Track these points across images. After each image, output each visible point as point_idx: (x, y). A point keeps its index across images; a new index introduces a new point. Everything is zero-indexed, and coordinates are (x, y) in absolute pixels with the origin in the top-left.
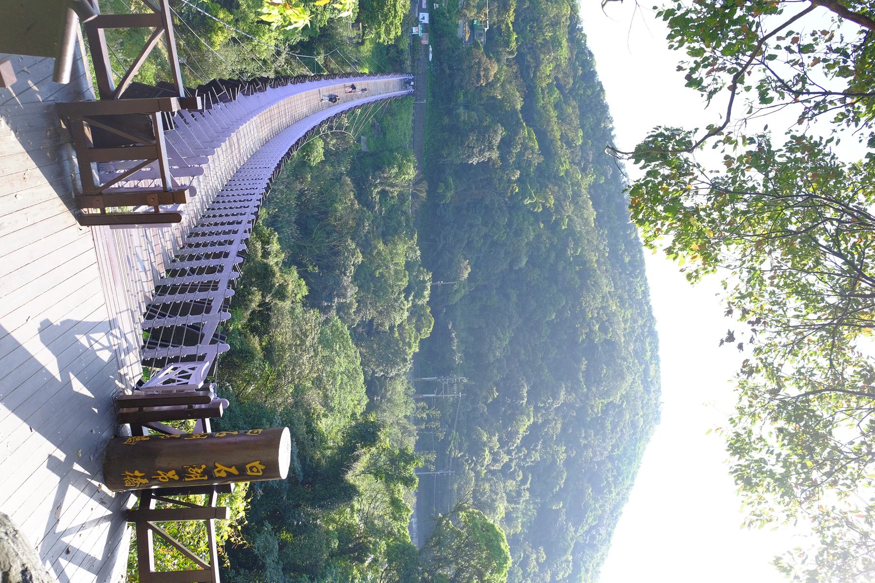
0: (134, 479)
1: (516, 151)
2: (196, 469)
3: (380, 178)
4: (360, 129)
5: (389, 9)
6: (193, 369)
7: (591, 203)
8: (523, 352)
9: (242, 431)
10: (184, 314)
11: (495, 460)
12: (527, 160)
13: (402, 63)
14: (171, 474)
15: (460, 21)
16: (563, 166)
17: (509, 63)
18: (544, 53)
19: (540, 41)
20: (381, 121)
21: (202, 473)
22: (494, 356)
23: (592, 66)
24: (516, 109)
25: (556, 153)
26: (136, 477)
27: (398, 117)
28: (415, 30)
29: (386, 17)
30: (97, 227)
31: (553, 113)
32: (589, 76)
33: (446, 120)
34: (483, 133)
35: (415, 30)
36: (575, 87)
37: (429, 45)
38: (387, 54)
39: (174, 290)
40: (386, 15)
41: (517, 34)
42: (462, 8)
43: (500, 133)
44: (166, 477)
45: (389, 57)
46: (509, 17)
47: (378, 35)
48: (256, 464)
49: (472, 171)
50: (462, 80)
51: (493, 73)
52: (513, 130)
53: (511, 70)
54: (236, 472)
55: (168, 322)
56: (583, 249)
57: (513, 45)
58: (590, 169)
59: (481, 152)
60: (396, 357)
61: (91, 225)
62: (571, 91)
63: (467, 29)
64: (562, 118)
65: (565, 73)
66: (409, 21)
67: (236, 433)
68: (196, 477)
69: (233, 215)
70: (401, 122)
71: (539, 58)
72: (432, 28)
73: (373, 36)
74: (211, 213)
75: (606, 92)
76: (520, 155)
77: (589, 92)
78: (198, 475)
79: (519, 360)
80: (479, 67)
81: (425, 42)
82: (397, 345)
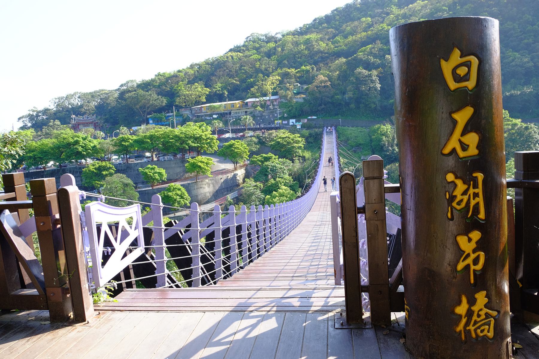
0: (475, 318)
1: (372, 59)
2: (458, 192)
3: (388, 147)
4: (356, 159)
5: (285, 141)
7: (411, 5)
8: (526, 41)
12: (379, 51)
13: (317, 134)
15: (294, 100)
16: (385, 28)
17: (319, 69)
18: (313, 49)
19: (306, 52)
20: (352, 147)
22: (528, 62)
23: (322, 18)
24: (346, 62)
25: (376, 34)
26: (470, 313)
27: (350, 136)
29: (289, 143)
31: (350, 38)
32: (328, 19)
33: (353, 106)
34: (360, 81)
36: (334, 27)
37: (307, 119)
38: (312, 143)
40: (288, 143)
41: (302, 66)
42: (287, 100)
43: (361, 71)
44: (473, 256)
45: (314, 142)
46: (292, 72)
47: (300, 148)
48: (447, 67)
49: (385, 87)
50: (328, 97)
51: (323, 78)
52: (359, 63)
53: (322, 68)
56: (443, 5)
57: (308, 68)
58: (387, 10)
59: (373, 81)
60: (524, 135)
62: (336, 29)
63: (299, 96)
64: (353, 32)
65: (326, 35)
66: (293, 130)
68: (476, 195)
70: (353, 134)
71: (316, 51)
72: (298, 117)
73: (300, 151)
75: (338, 7)
76: (375, 56)
77: (338, 17)
78: (471, 191)
79: (533, 43)
80: (320, 86)
81: (306, 121)
82: (513, 134)
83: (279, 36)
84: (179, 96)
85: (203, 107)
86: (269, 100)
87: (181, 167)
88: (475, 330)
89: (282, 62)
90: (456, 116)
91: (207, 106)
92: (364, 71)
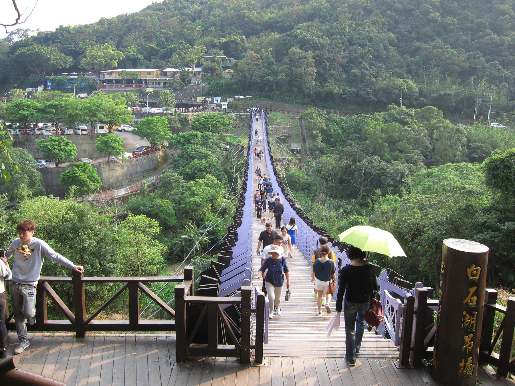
14: (467, 339)
26: (465, 366)
28: (224, 107)
35: (224, 107)
48: (469, 270)
54: (475, 288)
68: (473, 320)
84: (85, 57)
85: (114, 72)
86: (192, 72)
87: (90, 143)
88: (466, 373)
89: (208, 29)
90: (470, 289)
91: (118, 72)
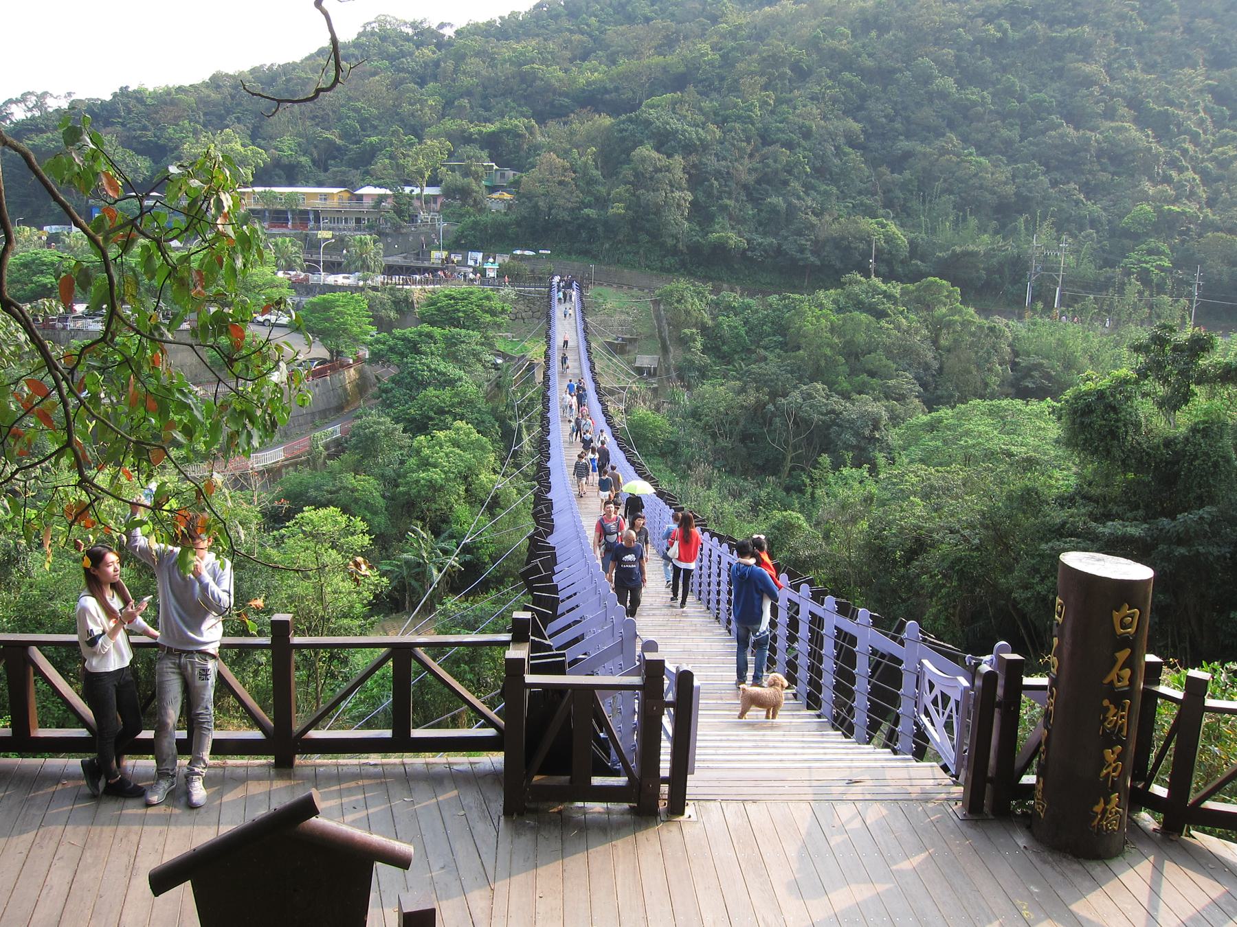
6: (932, 686)
7: (767, 9)
9: (1055, 631)
10: (852, 679)
11: (1192, 195)
14: (1110, 755)
21: (1117, 707)
26: (1104, 811)
30: (688, 791)
31: (624, 64)
39: (815, 685)
54: (1127, 651)
55: (861, 703)
61: (685, 799)
67: (1056, 640)
68: (1122, 717)
69: (719, 575)
74: (713, 605)
83: (448, 32)
92: (655, 154)
